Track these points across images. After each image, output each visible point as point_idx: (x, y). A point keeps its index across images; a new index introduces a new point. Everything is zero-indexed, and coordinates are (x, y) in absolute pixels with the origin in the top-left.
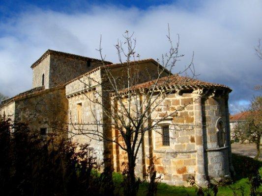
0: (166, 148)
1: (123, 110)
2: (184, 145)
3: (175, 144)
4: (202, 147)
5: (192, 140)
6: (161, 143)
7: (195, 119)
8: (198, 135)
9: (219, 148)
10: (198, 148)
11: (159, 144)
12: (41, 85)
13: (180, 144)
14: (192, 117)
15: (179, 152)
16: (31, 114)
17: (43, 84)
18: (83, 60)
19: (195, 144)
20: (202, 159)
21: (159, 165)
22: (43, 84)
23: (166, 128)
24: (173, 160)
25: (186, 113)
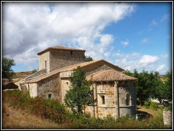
3: (106, 104)
4: (117, 106)
5: (114, 103)
6: (102, 103)
8: (116, 101)
9: (126, 106)
10: (116, 106)
11: (100, 104)
12: (45, 68)
15: (108, 108)
17: (46, 67)
22: (46, 67)
23: (103, 97)
24: (105, 110)
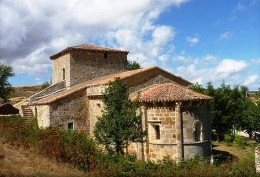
0: (159, 142)
1: (86, 164)
2: (169, 140)
5: (174, 137)
6: (155, 137)
7: (176, 122)
8: (178, 134)
10: (177, 142)
11: (153, 138)
13: (166, 139)
14: (174, 121)
15: (165, 145)
16: (61, 113)
17: (64, 78)
18: (101, 53)
19: (176, 139)
20: (181, 150)
21: (153, 153)
22: (64, 78)
24: (161, 150)
25: (170, 118)
